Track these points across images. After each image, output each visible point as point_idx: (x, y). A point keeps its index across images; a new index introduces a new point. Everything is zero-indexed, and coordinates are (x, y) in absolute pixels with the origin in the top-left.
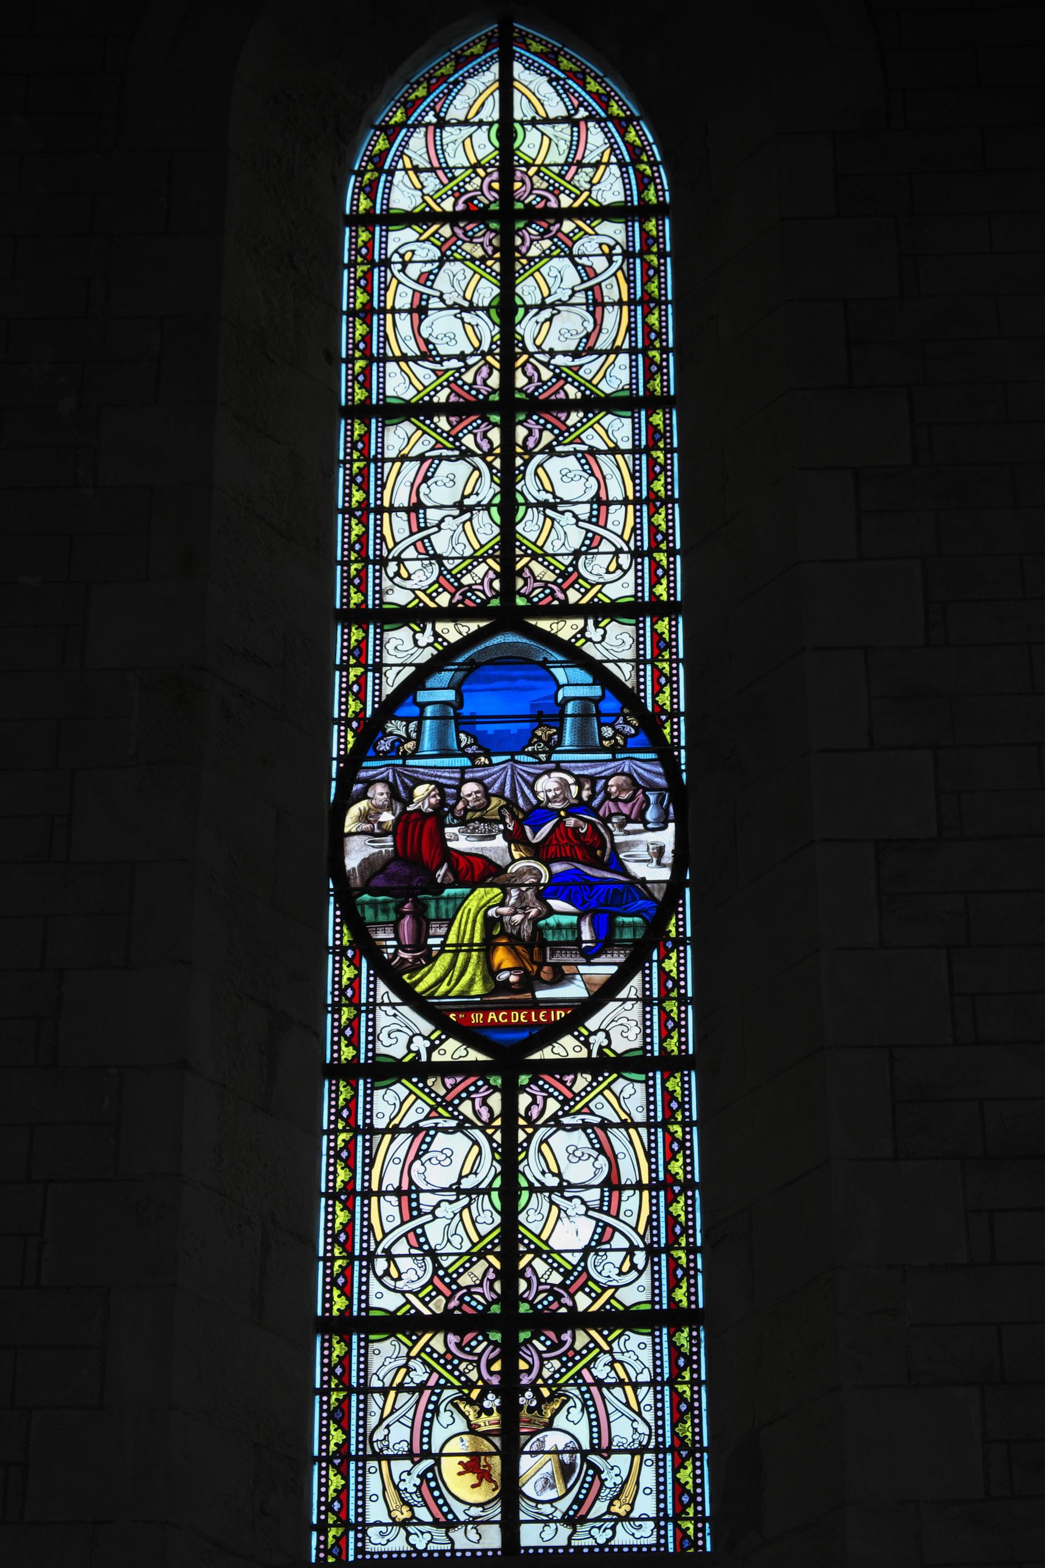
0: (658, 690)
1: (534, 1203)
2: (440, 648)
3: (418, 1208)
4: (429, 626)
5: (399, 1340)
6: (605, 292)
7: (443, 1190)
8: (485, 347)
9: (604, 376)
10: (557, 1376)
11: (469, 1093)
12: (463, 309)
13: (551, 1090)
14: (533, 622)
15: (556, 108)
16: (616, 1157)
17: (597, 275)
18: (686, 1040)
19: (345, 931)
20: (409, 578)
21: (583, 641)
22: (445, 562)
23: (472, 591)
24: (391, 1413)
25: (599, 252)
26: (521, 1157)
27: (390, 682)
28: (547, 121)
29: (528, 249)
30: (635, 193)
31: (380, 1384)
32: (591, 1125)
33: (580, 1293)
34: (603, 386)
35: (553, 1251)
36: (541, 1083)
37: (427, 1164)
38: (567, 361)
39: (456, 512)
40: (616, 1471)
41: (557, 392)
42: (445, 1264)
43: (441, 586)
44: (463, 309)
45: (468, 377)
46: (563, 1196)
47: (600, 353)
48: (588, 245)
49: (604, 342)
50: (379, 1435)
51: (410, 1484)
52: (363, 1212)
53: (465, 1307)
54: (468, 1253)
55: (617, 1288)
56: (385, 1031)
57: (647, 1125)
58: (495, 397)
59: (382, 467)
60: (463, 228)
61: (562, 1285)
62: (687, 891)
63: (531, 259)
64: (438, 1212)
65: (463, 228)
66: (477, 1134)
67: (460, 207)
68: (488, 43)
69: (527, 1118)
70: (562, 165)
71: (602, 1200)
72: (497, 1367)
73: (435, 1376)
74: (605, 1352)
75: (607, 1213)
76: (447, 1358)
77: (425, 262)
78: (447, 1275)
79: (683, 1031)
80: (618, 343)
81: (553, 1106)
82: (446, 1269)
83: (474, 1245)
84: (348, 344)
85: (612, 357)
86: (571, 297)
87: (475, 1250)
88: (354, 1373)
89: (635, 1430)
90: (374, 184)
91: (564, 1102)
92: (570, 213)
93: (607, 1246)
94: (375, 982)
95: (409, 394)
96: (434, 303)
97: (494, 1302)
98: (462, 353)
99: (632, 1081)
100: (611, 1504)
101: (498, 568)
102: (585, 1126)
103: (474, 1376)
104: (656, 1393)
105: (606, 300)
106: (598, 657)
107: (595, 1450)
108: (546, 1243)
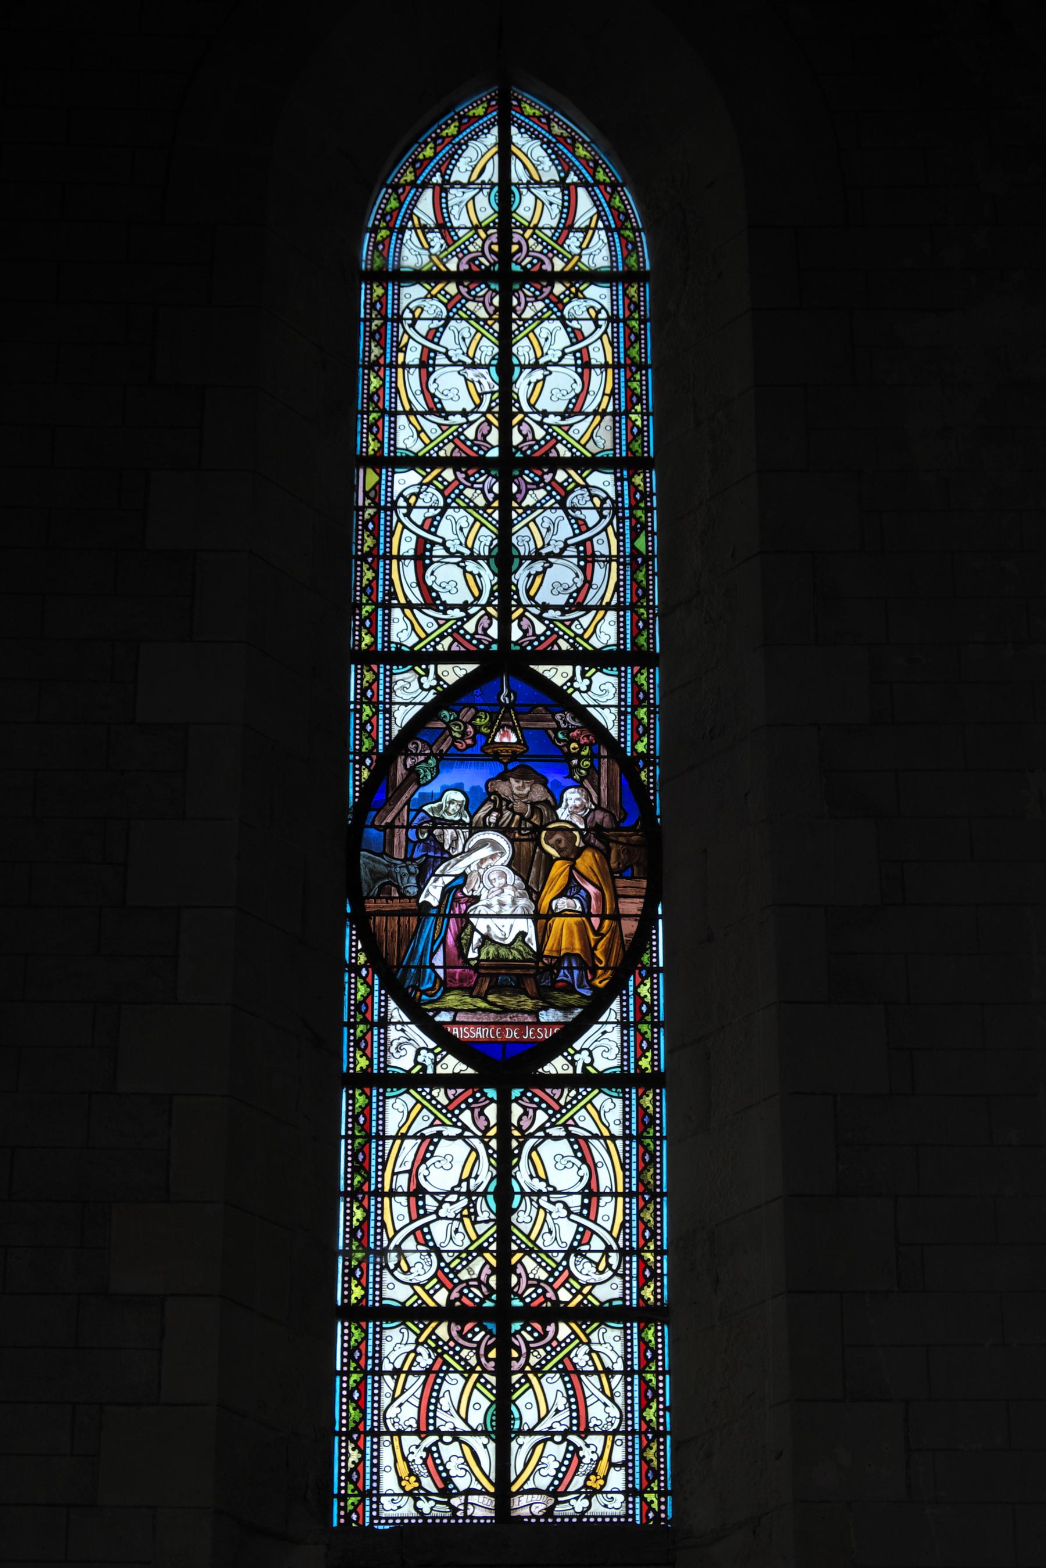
5: (408, 1328)
8: (483, 601)
9: (594, 631)
10: (543, 1362)
15: (549, 172)
17: (585, 338)
22: (444, 1255)
25: (586, 316)
26: (515, 1161)
27: (399, 722)
28: (540, 183)
33: (563, 1289)
37: (432, 1168)
38: (557, 420)
40: (593, 1448)
41: (552, 645)
44: (464, 558)
45: (470, 626)
46: (549, 1201)
48: (575, 308)
49: (593, 598)
50: (391, 1413)
51: (418, 1456)
53: (464, 1299)
55: (594, 1285)
56: (395, 1044)
59: (383, 1145)
63: (525, 321)
65: (465, 473)
66: (476, 1142)
67: (464, 267)
72: (493, 1354)
77: (429, 508)
80: (607, 599)
83: (472, 1242)
84: (356, 689)
86: (561, 359)
95: (416, 446)
96: (441, 360)
100: (587, 1479)
105: (593, 362)
106: (583, 702)
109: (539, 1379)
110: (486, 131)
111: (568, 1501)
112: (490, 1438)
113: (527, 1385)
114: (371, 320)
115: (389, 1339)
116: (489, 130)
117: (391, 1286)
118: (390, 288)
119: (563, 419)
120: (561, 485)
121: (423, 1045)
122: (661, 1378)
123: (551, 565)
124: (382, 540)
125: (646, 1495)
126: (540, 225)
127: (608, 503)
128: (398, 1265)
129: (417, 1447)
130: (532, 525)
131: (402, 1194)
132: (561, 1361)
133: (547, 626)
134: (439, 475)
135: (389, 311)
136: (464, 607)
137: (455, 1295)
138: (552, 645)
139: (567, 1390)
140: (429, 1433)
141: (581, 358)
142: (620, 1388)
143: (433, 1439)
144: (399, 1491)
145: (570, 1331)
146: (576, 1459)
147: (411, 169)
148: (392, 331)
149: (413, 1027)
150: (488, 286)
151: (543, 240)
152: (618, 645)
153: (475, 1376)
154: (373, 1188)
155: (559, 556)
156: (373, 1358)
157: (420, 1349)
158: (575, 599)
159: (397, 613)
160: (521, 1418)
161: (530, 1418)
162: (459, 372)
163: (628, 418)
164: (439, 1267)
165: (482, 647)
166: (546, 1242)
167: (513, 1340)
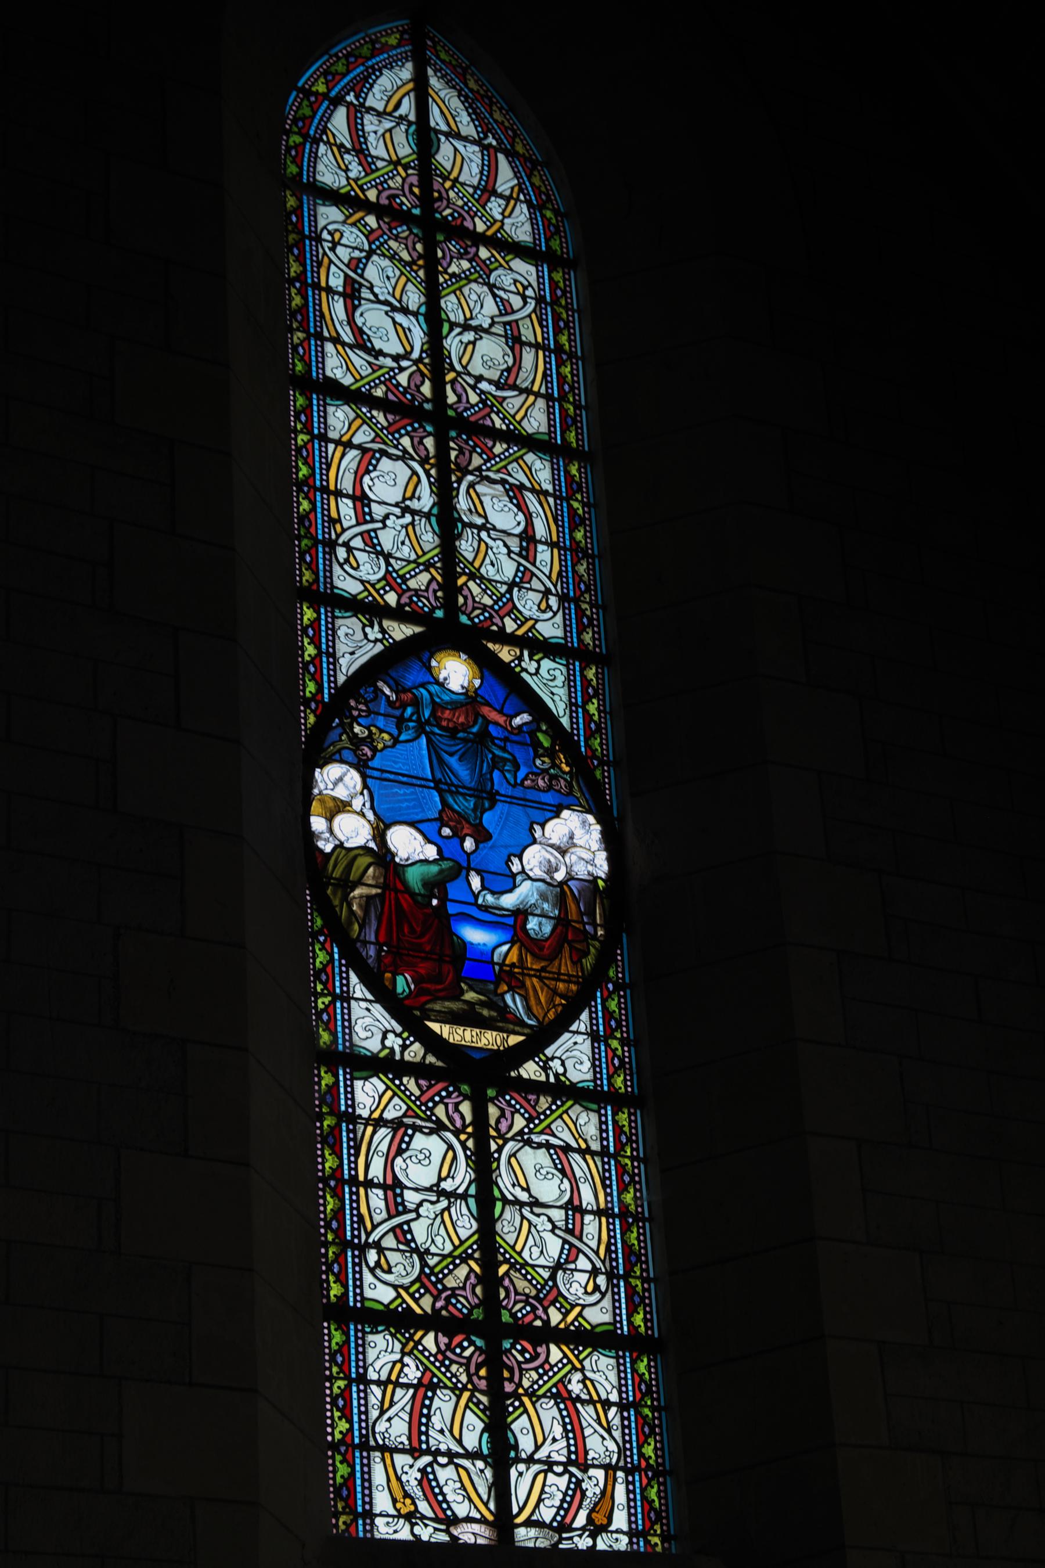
1: (507, 1215)
3: (403, 1203)
7: (427, 1189)
8: (415, 355)
12: (394, 309)
13: (518, 1107)
16: (531, 515)
27: (344, 671)
28: (458, 136)
29: (449, 265)
30: (554, 367)
32: (554, 1147)
37: (376, 480)
38: (491, 389)
39: (397, 511)
41: (484, 418)
43: (388, 584)
46: (532, 1212)
48: (503, 278)
50: (381, 1427)
51: (412, 1477)
52: (363, 1473)
54: (450, 1255)
55: (584, 1307)
62: (624, 935)
64: (421, 1210)
66: (449, 1135)
69: (497, 1130)
72: (483, 1372)
73: (428, 1374)
74: (576, 1370)
78: (432, 1273)
82: (432, 1269)
83: (456, 1248)
87: (456, 1253)
91: (530, 1120)
93: (572, 1266)
96: (365, 294)
97: (477, 1306)
99: (587, 1109)
102: (548, 1146)
109: (533, 1404)
110: (400, 63)
111: (571, 1538)
112: (487, 1463)
113: (521, 1409)
115: (372, 1344)
116: (403, 64)
118: (322, 610)
121: (389, 1028)
123: (481, 338)
125: (649, 1538)
129: (411, 1466)
132: (555, 1385)
135: (306, 229)
136: (396, 358)
138: (484, 418)
139: (563, 1417)
142: (617, 1421)
143: (427, 1459)
144: (393, 1512)
145: (561, 1355)
147: (322, 80)
148: (323, 503)
149: (378, 1006)
150: (409, 229)
153: (466, 1395)
157: (407, 1360)
161: (526, 1444)
162: (386, 313)
163: (607, 1045)
164: (387, 570)
166: (488, 571)
167: (504, 1358)
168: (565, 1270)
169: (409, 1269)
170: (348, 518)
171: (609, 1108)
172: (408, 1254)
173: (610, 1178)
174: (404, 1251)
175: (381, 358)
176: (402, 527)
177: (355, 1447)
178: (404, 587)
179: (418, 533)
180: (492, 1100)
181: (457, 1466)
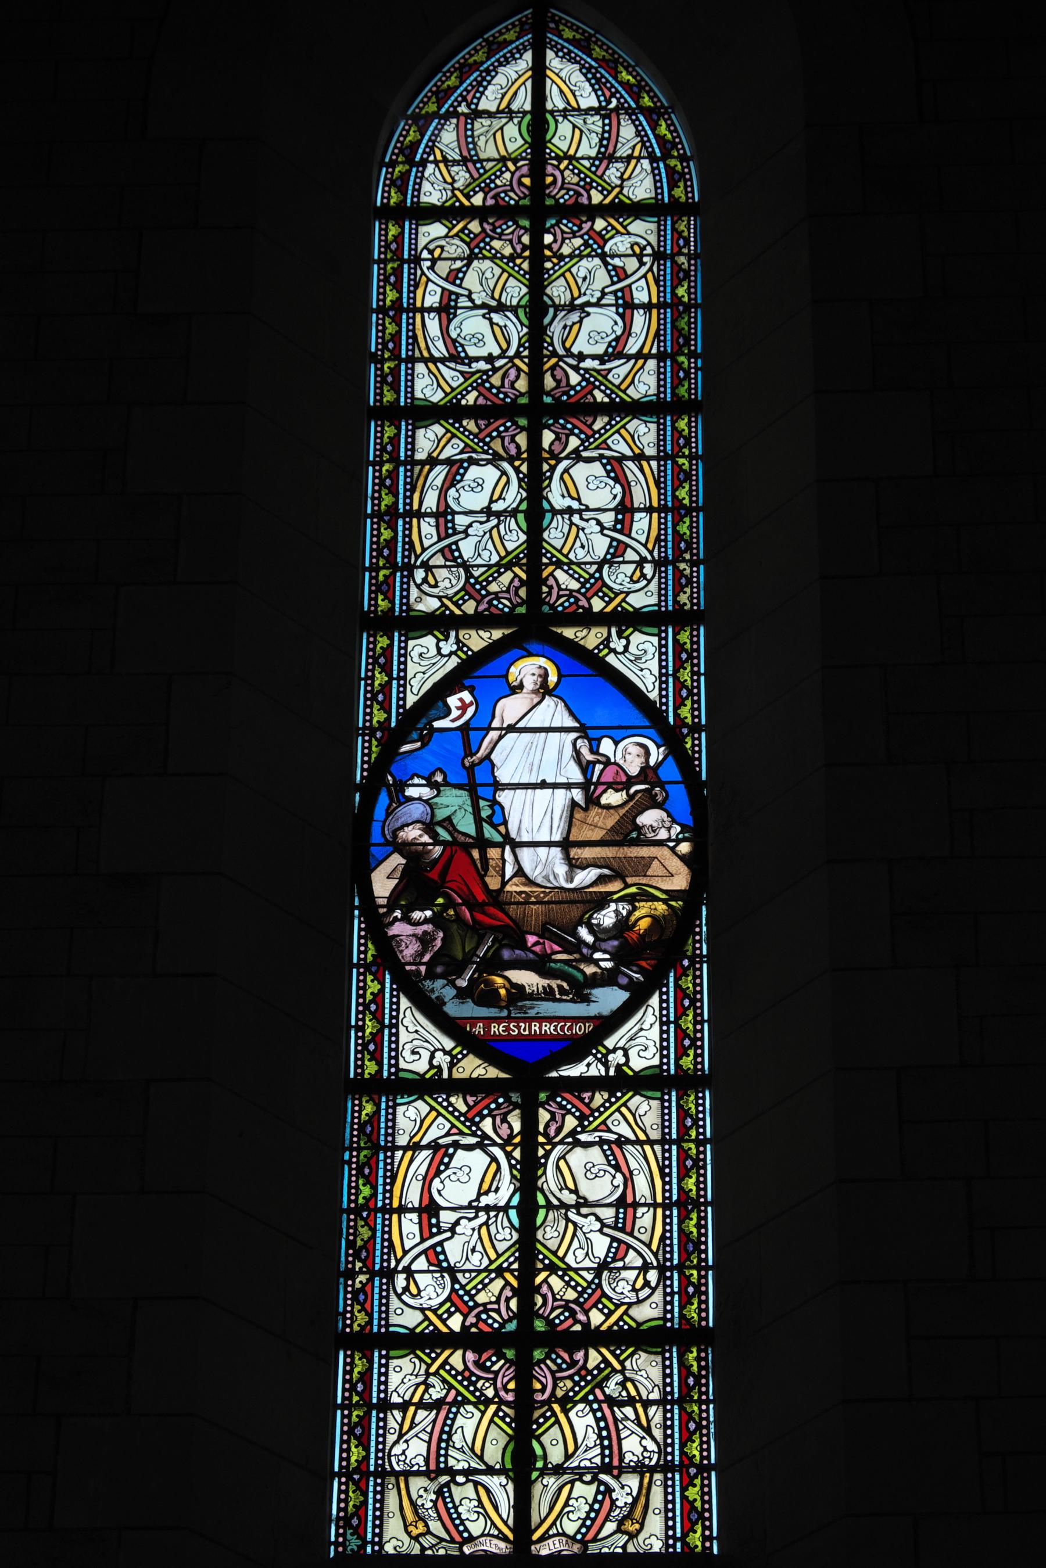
0: (679, 703)
2: (464, 656)
3: (453, 528)
4: (453, 634)
6: (636, 294)
7: (462, 1208)
8: (511, 352)
9: (633, 382)
11: (499, 433)
12: (492, 310)
14: (554, 1074)
15: (589, 100)
17: (627, 277)
18: (701, 1059)
19: (370, 945)
20: (436, 586)
21: (606, 651)
22: (459, 1276)
23: (486, 1311)
24: (411, 1428)
25: (630, 252)
26: (540, 1172)
31: (400, 1400)
32: (608, 1142)
33: (594, 1310)
34: (631, 391)
35: (571, 562)
36: (559, 1099)
42: (476, 574)
45: (496, 380)
46: (579, 1214)
47: (629, 357)
48: (620, 244)
49: (633, 347)
53: (481, 1325)
54: (486, 1270)
55: (630, 1305)
57: (658, 458)
58: (524, 400)
59: (392, 1157)
60: (493, 224)
61: (576, 1301)
62: (704, 908)
65: (493, 224)
66: (506, 465)
67: (490, 202)
68: (521, 29)
70: (594, 159)
71: (617, 1217)
73: (453, 1392)
75: (622, 1230)
76: (466, 1376)
77: (455, 259)
79: (703, 1298)
81: (571, 1122)
82: (476, 579)
83: (491, 1262)
85: (641, 362)
87: (493, 1267)
88: (404, 347)
89: (645, 1449)
90: (405, 176)
91: (581, 1118)
92: (601, 211)
93: (620, 1264)
94: (398, 997)
96: (463, 302)
98: (490, 354)
99: (648, 1098)
101: (524, 576)
103: (490, 1393)
104: (665, 1411)
107: (606, 1468)
108: (562, 1259)
112: (508, 1477)
114: (381, 464)
117: (399, 1311)
119: (603, 363)
120: (599, 234)
122: (704, 1407)
123: (588, 314)
124: (380, 1189)
126: (579, 155)
127: (649, 250)
128: (406, 1289)
130: (568, 275)
131: (413, 1210)
133: (582, 376)
134: (465, 228)
137: (471, 1319)
140: (439, 1472)
141: (623, 298)
145: (600, 1358)
146: (607, 1501)
150: (516, 223)
151: (580, 172)
152: (657, 395)
153: (493, 1408)
154: (380, 1204)
155: (597, 304)
156: (373, 1543)
157: (432, 1380)
158: (614, 348)
159: (420, 368)
160: (545, 1456)
162: (484, 316)
164: (453, 1290)
165: (508, 400)
168: (611, 1270)
169: (454, 582)
170: (411, 1236)
171: (674, 1093)
172: (437, 1275)
173: (670, 1166)
174: (450, 567)
175: (474, 365)
176: (473, 1230)
177: (377, 1210)
178: (471, 1304)
179: (503, 533)
180: (542, 1105)
181: (476, 1484)
